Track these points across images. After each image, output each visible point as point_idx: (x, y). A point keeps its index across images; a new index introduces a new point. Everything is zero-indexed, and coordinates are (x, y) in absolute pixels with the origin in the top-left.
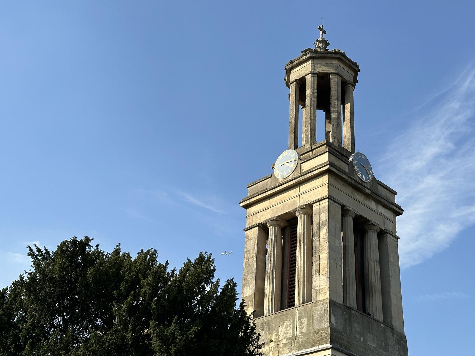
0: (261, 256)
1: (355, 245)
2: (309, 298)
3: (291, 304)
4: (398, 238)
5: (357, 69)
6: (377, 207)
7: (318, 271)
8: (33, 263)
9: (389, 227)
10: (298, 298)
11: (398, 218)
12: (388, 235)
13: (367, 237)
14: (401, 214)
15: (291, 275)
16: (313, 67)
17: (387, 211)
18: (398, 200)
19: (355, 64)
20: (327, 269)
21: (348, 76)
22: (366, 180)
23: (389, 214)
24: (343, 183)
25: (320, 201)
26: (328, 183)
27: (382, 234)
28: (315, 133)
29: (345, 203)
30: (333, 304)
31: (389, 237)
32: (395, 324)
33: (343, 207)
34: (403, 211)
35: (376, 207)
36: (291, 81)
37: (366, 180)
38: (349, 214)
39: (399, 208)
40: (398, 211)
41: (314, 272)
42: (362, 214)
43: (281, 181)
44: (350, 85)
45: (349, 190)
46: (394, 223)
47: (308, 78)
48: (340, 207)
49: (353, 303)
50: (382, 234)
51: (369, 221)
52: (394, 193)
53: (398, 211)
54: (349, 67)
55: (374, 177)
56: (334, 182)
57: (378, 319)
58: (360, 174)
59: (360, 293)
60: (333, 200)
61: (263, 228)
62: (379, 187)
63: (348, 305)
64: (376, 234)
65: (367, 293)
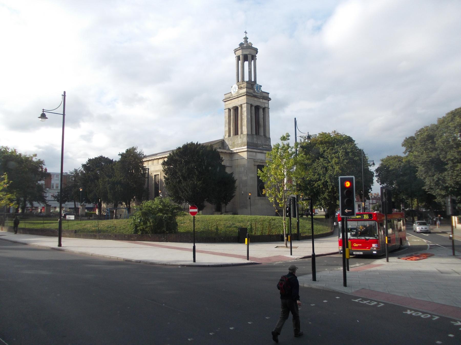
2: (242, 133)
3: (238, 134)
6: (262, 100)
8: (229, 202)
9: (266, 106)
10: (239, 133)
13: (198, 249)
16: (242, 52)
17: (266, 100)
18: (270, 96)
19: (256, 48)
20: (246, 125)
26: (245, 102)
27: (264, 109)
28: (242, 89)
30: (248, 134)
32: (267, 135)
41: (243, 126)
42: (257, 105)
43: (233, 96)
47: (241, 56)
49: (254, 133)
50: (264, 109)
51: (260, 106)
53: (269, 99)
54: (254, 50)
56: (248, 97)
57: (262, 135)
61: (229, 110)
62: (263, 93)
64: (262, 109)
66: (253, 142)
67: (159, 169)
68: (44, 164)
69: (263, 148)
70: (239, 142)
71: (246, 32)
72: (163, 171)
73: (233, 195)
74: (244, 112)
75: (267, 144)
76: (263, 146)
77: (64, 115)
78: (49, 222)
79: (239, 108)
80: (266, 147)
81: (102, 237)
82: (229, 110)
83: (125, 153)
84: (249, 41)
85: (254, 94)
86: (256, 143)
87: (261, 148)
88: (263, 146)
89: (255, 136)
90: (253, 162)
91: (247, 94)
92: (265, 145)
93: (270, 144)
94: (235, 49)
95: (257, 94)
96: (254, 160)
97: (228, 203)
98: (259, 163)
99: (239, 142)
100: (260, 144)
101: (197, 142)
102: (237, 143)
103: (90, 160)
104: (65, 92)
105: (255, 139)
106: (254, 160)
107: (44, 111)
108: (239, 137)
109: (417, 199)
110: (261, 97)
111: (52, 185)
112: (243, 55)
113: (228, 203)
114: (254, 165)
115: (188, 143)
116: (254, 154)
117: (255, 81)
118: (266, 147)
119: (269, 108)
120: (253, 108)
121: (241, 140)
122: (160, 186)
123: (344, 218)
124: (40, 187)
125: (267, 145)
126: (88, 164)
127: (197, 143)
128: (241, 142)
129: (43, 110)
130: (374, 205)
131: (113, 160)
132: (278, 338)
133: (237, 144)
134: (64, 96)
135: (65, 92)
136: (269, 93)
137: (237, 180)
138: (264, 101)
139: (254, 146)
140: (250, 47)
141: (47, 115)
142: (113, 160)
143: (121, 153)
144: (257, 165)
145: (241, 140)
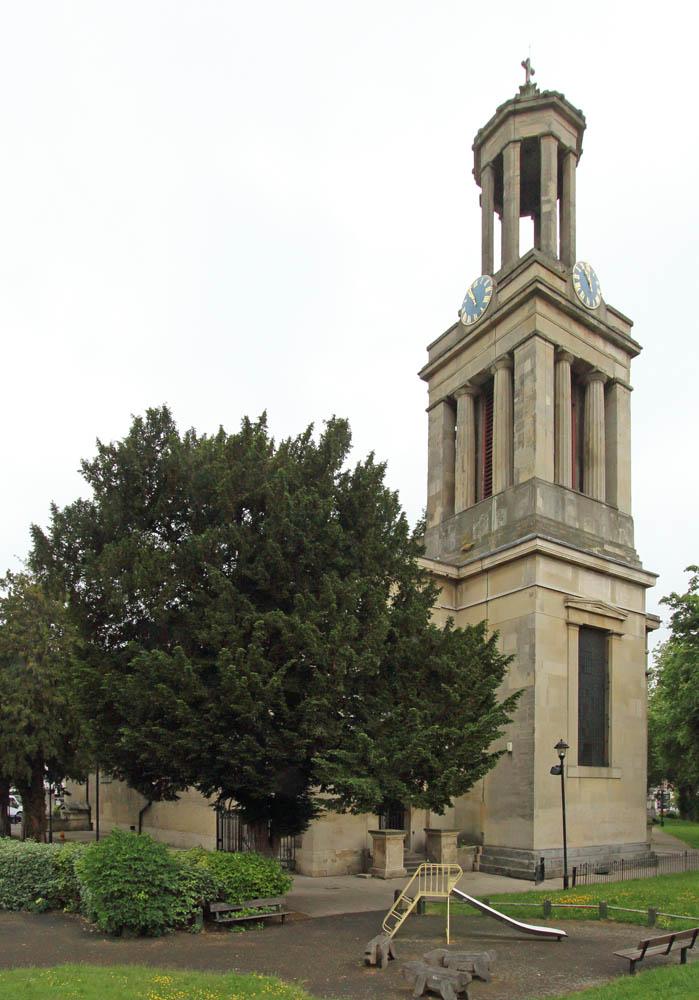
0: (449, 441)
1: (573, 405)
4: (631, 390)
5: (581, 123)
7: (521, 443)
11: (634, 361)
12: (618, 385)
14: (638, 354)
15: (486, 481)
17: (619, 351)
18: (635, 334)
19: (579, 114)
21: (569, 141)
22: (591, 305)
23: (620, 356)
24: (557, 311)
25: (524, 342)
27: (610, 385)
29: (560, 342)
31: (619, 389)
32: (620, 504)
33: (556, 347)
34: (641, 348)
35: (533, 620)
36: (482, 166)
37: (591, 305)
38: (566, 357)
39: (635, 344)
40: (632, 352)
41: (516, 445)
43: (469, 329)
44: (571, 155)
45: (566, 322)
46: (627, 368)
48: (552, 347)
49: (568, 481)
50: (610, 385)
51: (593, 367)
52: (630, 324)
53: (632, 352)
55: (602, 301)
58: (582, 296)
59: (577, 469)
60: (555, 292)
61: (451, 402)
63: (561, 483)
64: (602, 385)
65: (586, 469)
66: (563, 519)
70: (495, 527)
71: (525, 64)
73: (490, 751)
74: (522, 383)
76: (607, 548)
79: (500, 378)
80: (617, 551)
87: (595, 550)
88: (607, 548)
89: (570, 496)
90: (564, 610)
91: (383, 836)
92: (611, 543)
93: (629, 545)
96: (566, 601)
97: (452, 799)
98: (586, 615)
99: (495, 527)
100: (593, 535)
102: (486, 531)
105: (571, 511)
106: (568, 598)
108: (495, 504)
113: (452, 799)
114: (569, 624)
116: (569, 571)
117: (568, 255)
118: (617, 551)
119: (631, 390)
121: (505, 517)
123: (386, 828)
125: (619, 546)
128: (502, 524)
130: (245, 832)
132: (207, 430)
137: (511, 659)
140: (554, 103)
144: (581, 623)
145: (504, 512)
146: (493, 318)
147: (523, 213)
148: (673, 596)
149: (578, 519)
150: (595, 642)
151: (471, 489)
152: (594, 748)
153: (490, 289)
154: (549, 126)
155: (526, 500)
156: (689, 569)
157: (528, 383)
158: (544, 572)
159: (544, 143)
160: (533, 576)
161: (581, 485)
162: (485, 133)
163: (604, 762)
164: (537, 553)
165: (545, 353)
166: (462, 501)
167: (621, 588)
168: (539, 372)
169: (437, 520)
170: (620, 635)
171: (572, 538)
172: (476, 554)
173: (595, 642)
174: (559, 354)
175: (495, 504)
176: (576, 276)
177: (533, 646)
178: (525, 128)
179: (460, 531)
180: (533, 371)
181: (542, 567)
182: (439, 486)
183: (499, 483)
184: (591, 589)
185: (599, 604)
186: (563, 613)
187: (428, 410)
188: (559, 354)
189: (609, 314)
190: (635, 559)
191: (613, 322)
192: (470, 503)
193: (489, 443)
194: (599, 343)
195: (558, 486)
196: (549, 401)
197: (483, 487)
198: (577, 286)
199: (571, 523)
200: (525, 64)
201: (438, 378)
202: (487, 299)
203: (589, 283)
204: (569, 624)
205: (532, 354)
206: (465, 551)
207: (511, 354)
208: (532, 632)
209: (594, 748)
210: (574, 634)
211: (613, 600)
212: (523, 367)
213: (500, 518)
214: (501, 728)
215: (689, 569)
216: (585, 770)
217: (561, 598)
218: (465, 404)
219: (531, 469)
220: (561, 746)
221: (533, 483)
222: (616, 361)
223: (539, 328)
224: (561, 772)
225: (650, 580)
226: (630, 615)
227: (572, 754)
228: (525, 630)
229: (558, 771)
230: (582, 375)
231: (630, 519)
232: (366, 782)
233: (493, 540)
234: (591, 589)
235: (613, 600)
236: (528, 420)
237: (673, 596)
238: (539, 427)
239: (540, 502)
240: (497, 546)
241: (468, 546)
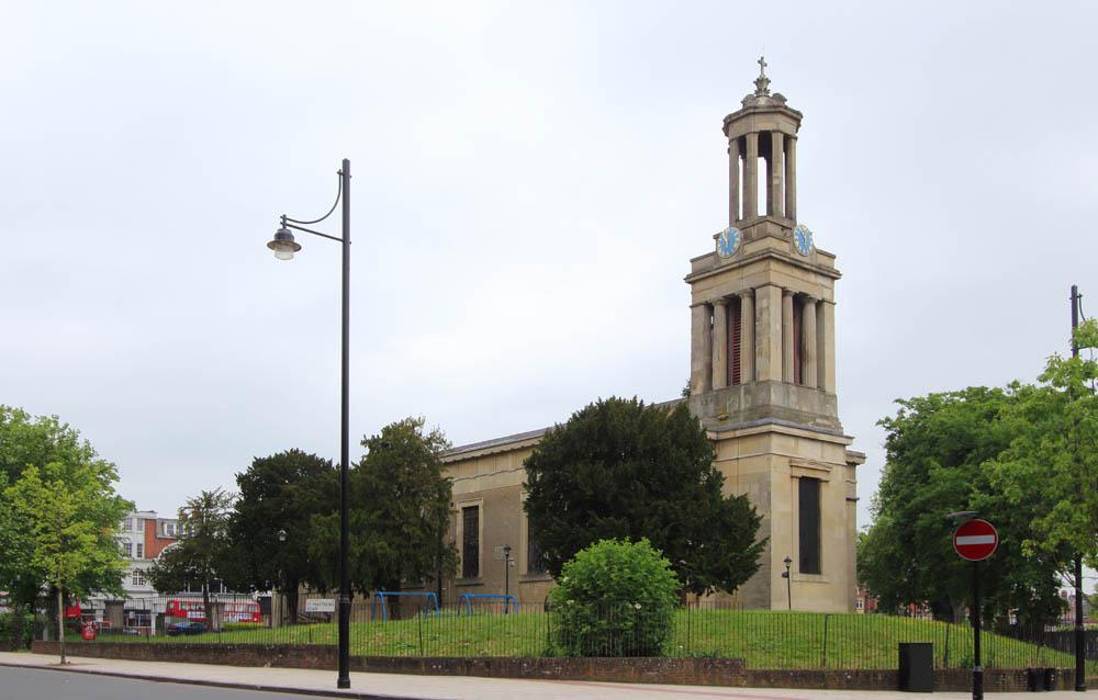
1: (794, 317)
4: (834, 304)
9: (826, 295)
18: (837, 266)
19: (798, 113)
27: (819, 304)
31: (826, 306)
32: (828, 389)
40: (833, 276)
46: (832, 289)
49: (791, 379)
50: (819, 304)
53: (833, 276)
59: (798, 361)
61: (710, 307)
67: (478, 490)
68: (116, 478)
69: (818, 425)
70: (743, 407)
71: (761, 62)
72: (524, 485)
75: (828, 414)
76: (818, 421)
77: (345, 241)
78: (112, 645)
79: (746, 303)
81: (437, 668)
82: (710, 307)
83: (381, 437)
84: (773, 89)
85: (792, 256)
86: (797, 408)
87: (810, 425)
88: (818, 421)
89: (793, 388)
92: (822, 417)
94: (730, 116)
95: (800, 258)
96: (791, 462)
97: (738, 586)
99: (743, 407)
101: (635, 398)
102: (736, 408)
103: (259, 463)
104: (346, 163)
105: (793, 398)
107: (288, 222)
109: (1046, 622)
110: (814, 269)
111: (143, 531)
112: (735, 142)
114: (792, 477)
115: (604, 400)
116: (792, 442)
117: (791, 215)
119: (834, 304)
120: (789, 300)
122: (484, 542)
124: (409, 444)
125: (826, 418)
126: (254, 473)
127: (557, 426)
129: (284, 218)
131: (330, 462)
133: (735, 412)
134: (345, 174)
135: (346, 163)
136: (834, 257)
138: (821, 280)
139: (789, 419)
140: (778, 107)
141: (298, 236)
142: (330, 462)
143: (369, 438)
144: (800, 476)
145: (750, 399)
146: (742, 263)
147: (760, 155)
148: (888, 420)
149: (798, 403)
150: (810, 489)
151: (724, 373)
152: (810, 561)
153: (738, 239)
154: (778, 124)
155: (764, 394)
156: (897, 401)
157: (765, 316)
158: (776, 444)
159: (774, 135)
160: (769, 447)
161: (800, 378)
162: (733, 118)
163: (803, 480)
164: (770, 433)
165: (776, 294)
166: (719, 380)
167: (828, 448)
168: (772, 309)
169: (698, 391)
170: (827, 482)
171: (795, 417)
172: (729, 424)
173: (810, 489)
174: (785, 292)
175: (743, 391)
176: (796, 237)
177: (769, 494)
178: (763, 124)
179: (717, 404)
180: (768, 308)
181: (775, 440)
182: (700, 366)
183: (745, 376)
184: (809, 452)
185: (814, 463)
186: (788, 470)
187: (691, 307)
188: (785, 292)
189: (819, 255)
190: (838, 426)
191: (822, 260)
192: (724, 386)
193: (737, 339)
194: (812, 277)
195: (785, 383)
196: (779, 327)
197: (733, 377)
198: (797, 243)
199: (793, 406)
200: (761, 62)
201: (700, 286)
202: (736, 246)
203: (806, 236)
204: (792, 477)
205: (768, 296)
206: (721, 419)
207: (753, 290)
208: (769, 484)
209: (810, 561)
210: (796, 483)
211: (823, 457)
212: (761, 303)
213: (746, 401)
214: (760, 554)
215: (897, 401)
216: (805, 577)
217: (787, 460)
218: (719, 311)
219: (767, 373)
220: (788, 561)
221: (767, 383)
222: (823, 286)
223: (772, 280)
224: (788, 576)
225: (849, 441)
226: (835, 468)
227: (795, 565)
228: (764, 482)
229: (786, 575)
230: (800, 301)
231: (834, 397)
232: (922, 494)
233: (742, 417)
234: (809, 452)
235: (823, 457)
236: (765, 341)
237: (888, 420)
238: (772, 345)
239: (773, 397)
240: (745, 420)
241: (723, 416)
